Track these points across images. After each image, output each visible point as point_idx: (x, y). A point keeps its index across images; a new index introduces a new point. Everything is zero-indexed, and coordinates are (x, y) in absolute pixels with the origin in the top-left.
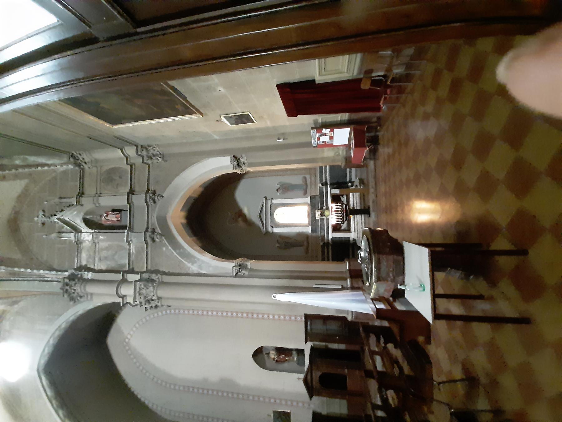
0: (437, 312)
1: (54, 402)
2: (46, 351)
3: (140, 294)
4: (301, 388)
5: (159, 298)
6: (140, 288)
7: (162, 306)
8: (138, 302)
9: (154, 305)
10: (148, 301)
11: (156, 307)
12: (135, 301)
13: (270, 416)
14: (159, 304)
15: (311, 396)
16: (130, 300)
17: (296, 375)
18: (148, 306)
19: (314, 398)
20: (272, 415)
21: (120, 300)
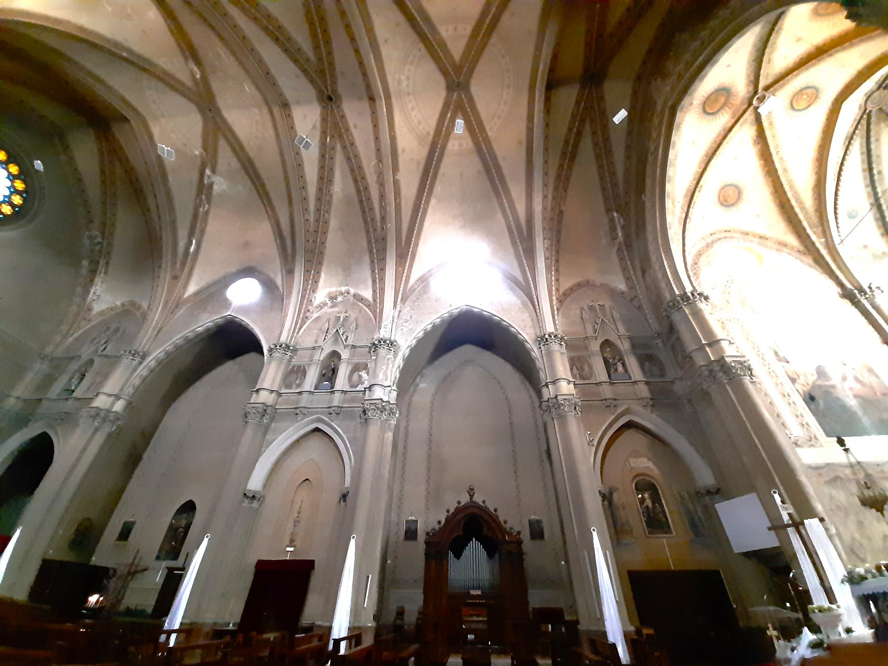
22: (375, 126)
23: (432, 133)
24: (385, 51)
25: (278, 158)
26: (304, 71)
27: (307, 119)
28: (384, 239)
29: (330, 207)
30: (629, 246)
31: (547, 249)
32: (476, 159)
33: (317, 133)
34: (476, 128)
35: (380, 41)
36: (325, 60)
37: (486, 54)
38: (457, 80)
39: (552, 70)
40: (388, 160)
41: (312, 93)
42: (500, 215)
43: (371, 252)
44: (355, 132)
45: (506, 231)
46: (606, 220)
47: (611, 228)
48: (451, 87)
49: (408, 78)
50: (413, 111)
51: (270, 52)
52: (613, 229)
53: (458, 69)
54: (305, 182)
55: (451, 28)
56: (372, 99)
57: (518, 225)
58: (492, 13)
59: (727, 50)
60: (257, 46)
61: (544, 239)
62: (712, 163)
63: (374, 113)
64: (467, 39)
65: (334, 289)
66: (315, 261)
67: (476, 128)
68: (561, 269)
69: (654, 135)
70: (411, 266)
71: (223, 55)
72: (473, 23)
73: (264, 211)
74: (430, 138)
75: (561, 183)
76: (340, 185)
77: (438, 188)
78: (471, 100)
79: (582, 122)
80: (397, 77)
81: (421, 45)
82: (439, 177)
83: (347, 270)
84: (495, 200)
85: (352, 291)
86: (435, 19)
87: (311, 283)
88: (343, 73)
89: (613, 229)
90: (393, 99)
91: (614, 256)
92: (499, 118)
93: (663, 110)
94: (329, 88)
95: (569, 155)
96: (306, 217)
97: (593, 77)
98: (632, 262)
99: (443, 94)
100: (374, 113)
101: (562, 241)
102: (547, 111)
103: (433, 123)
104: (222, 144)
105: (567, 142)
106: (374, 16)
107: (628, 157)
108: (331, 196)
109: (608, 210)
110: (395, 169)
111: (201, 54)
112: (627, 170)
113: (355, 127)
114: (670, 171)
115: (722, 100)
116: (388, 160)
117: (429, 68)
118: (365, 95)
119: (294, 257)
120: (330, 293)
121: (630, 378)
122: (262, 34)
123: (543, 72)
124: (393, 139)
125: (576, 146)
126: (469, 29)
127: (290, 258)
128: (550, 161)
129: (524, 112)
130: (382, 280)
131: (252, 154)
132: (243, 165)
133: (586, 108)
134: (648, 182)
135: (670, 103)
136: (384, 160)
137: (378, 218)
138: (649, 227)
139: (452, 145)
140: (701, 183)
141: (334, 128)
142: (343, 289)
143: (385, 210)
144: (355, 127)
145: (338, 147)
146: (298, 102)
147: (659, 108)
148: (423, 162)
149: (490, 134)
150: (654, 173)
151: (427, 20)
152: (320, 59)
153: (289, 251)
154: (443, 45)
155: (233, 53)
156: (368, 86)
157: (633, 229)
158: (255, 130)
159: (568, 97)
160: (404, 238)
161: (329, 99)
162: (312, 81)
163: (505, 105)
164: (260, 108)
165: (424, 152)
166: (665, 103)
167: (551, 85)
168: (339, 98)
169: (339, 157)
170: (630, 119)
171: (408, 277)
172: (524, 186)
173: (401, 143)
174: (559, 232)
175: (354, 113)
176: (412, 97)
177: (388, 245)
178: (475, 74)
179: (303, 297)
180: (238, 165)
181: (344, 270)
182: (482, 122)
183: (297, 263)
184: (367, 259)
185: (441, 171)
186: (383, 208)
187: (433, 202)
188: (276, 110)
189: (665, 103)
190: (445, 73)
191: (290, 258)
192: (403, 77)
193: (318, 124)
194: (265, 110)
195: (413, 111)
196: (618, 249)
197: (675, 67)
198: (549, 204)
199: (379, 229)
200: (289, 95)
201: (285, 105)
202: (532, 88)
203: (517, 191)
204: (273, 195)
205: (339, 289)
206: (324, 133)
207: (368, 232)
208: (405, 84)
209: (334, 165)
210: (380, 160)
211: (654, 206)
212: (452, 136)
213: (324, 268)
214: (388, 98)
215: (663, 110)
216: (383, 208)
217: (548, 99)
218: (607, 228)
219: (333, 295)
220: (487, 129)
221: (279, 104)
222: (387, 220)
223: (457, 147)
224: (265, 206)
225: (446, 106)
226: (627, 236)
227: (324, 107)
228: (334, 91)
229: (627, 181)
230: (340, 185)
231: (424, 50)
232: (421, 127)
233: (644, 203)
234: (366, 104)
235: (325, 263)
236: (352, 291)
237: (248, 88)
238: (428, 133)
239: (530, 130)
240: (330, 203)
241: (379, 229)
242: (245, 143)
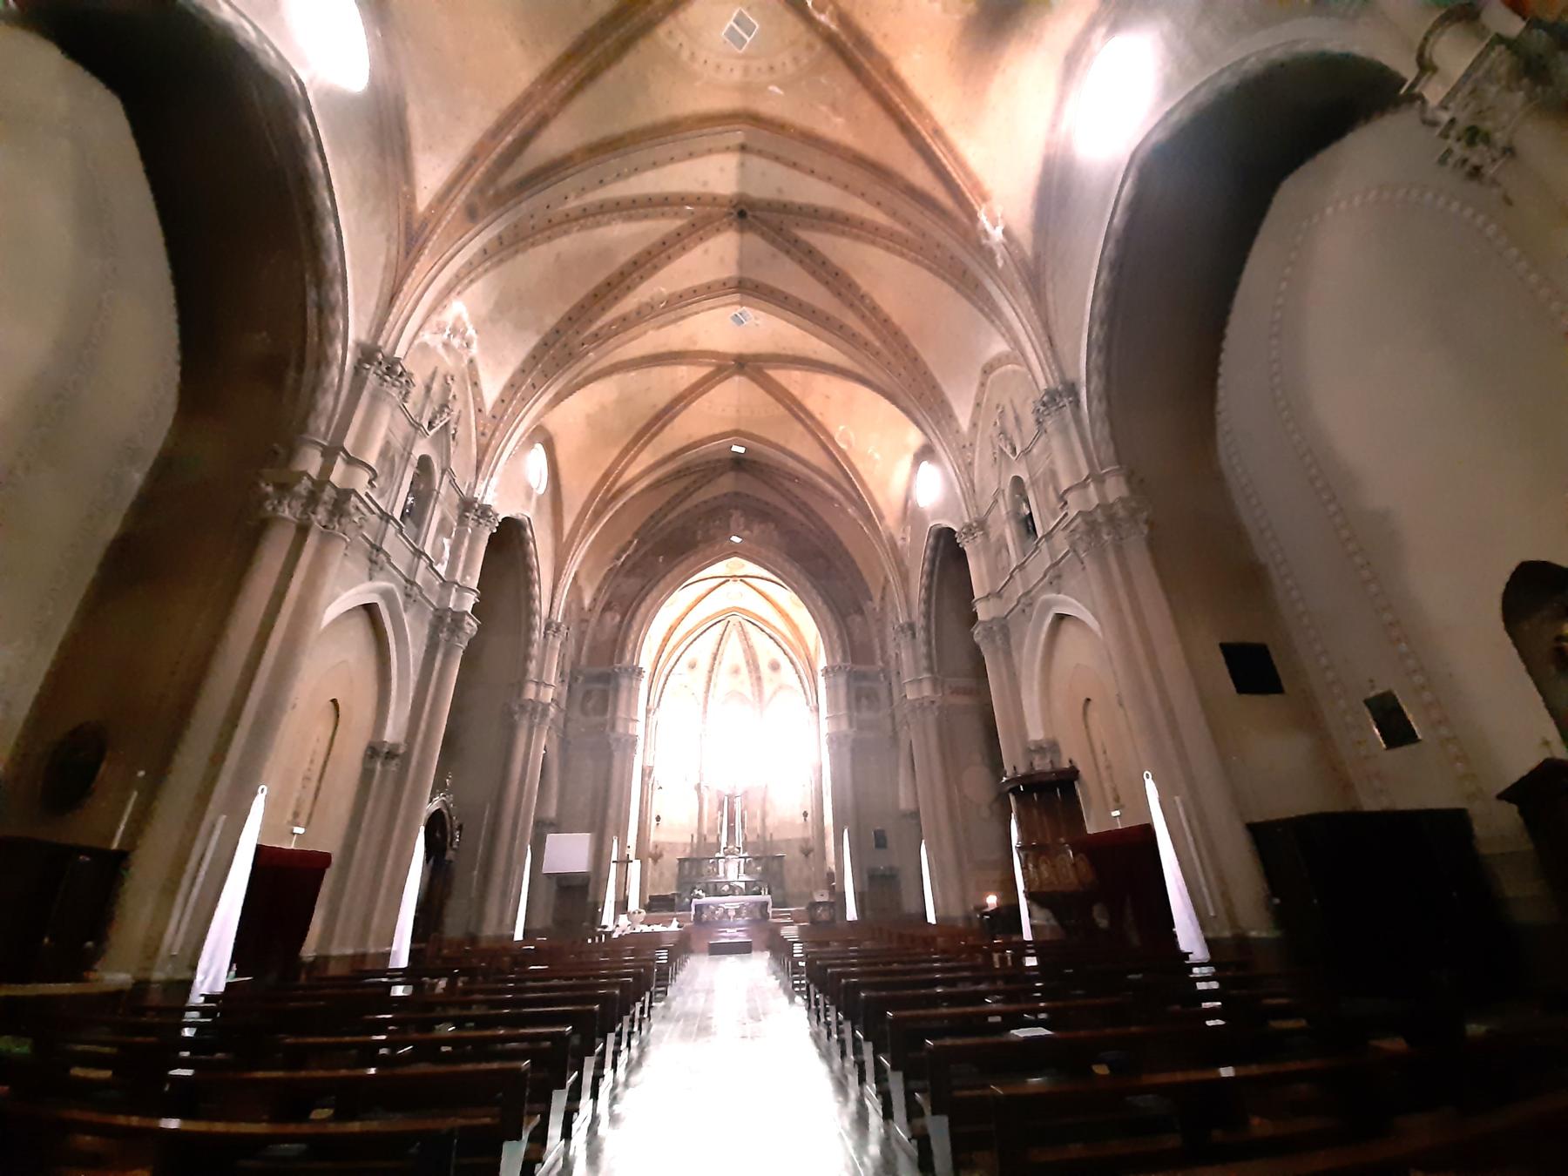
0: (454, 927)
1: (1110, 245)
2: (1175, 117)
3: (1473, 92)
4: (1520, 762)
5: (1509, 151)
6: (1489, 72)
7: (1494, 182)
8: (1445, 117)
9: (1475, 160)
10: (1473, 135)
11: (1476, 173)
12: (1443, 106)
13: (1373, 688)
14: (1490, 171)
15: (1509, 795)
16: (1434, 92)
17: (1552, 733)
18: (1459, 150)
19: (1510, 812)
20: (1379, 691)
21: (1408, 71)
23: (697, 348)
42: (615, 452)
46: (629, 537)
72: (799, 398)
74: (692, 348)
76: (686, 375)
83: (505, 308)
84: (631, 436)
89: (624, 551)
96: (572, 196)
104: (780, 376)
109: (636, 534)
121: (416, 541)
144: (706, 251)
145: (678, 223)
181: (497, 304)
184: (533, 340)
203: (646, 459)
206: (698, 200)
228: (752, 228)
230: (628, 237)
236: (475, 350)
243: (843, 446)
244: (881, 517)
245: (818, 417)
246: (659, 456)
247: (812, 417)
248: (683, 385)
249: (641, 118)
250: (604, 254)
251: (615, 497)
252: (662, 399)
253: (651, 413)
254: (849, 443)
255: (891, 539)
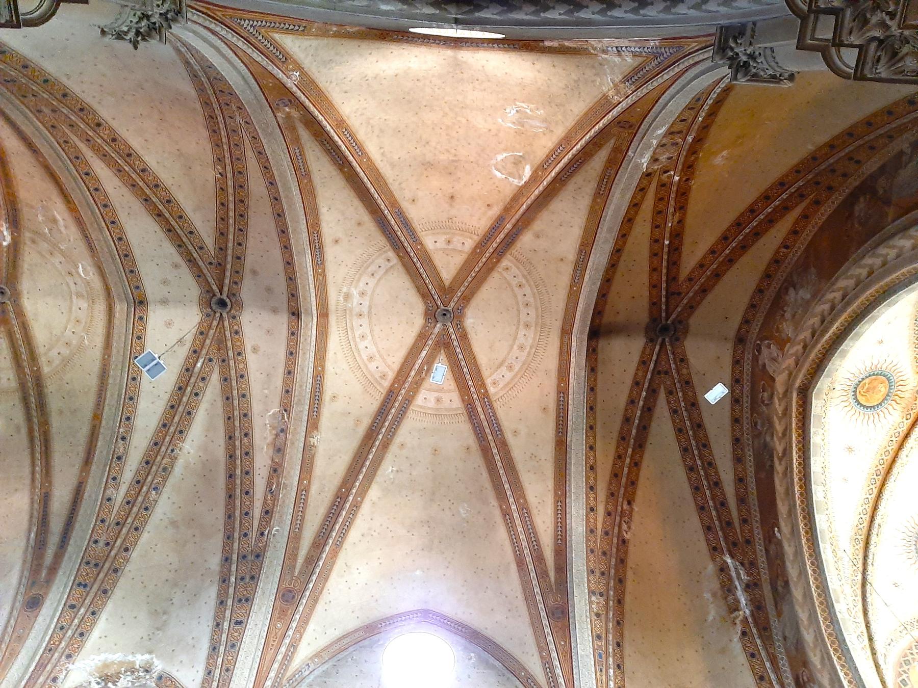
22: (291, 354)
23: (391, 376)
24: (331, 253)
25: (94, 382)
26: (191, 261)
27: (172, 328)
28: (259, 556)
29: (165, 479)
30: (764, 629)
31: (598, 615)
32: (464, 428)
33: (183, 352)
34: (468, 378)
35: (327, 239)
36: (230, 252)
37: (494, 280)
38: (445, 308)
39: (598, 312)
40: (301, 410)
41: (194, 290)
42: (502, 533)
43: (224, 580)
44: (252, 361)
45: (514, 567)
46: (711, 568)
47: (723, 586)
48: (431, 315)
49: (363, 294)
50: (366, 327)
51: (142, 232)
52: (727, 589)
53: (447, 292)
54: (130, 429)
55: (442, 239)
56: (295, 314)
57: (539, 558)
58: (506, 231)
59: (874, 319)
60: (123, 217)
61: (592, 592)
62: (890, 486)
63: (293, 334)
64: (464, 257)
65: (118, 657)
66: (99, 577)
67: (468, 378)
68: (628, 664)
69: (779, 427)
70: (305, 621)
71: (61, 222)
73: (27, 470)
74: (386, 384)
75: (622, 486)
76: (200, 439)
77: (387, 469)
78: (464, 337)
79: (653, 392)
80: (345, 290)
81: (391, 254)
82: (394, 448)
84: (494, 502)
85: (159, 666)
86: (417, 225)
87: (71, 636)
88: (254, 272)
89: (727, 589)
90: (332, 319)
91: (736, 646)
92: (510, 368)
93: (787, 393)
94: (226, 289)
95: (633, 439)
97: (666, 326)
98: (773, 660)
99: (419, 321)
100: (293, 334)
101: (628, 599)
102: (592, 369)
103: (396, 360)
105: (627, 420)
106: (323, 210)
107: (738, 460)
108: (174, 459)
109: (715, 550)
110: (313, 424)
111: (26, 213)
112: (740, 480)
113: (255, 350)
114: (818, 493)
115: (883, 390)
116: (301, 410)
117: (400, 282)
118: (285, 306)
119: (53, 570)
120: (106, 665)
122: (137, 205)
123: (585, 310)
124: (319, 378)
125: (644, 429)
126: (469, 244)
127: (44, 573)
128: (599, 446)
129: (551, 360)
130: (233, 646)
131: (46, 370)
132: (23, 386)
133: (657, 372)
134: (782, 508)
135: (798, 383)
136: (295, 410)
137: (257, 512)
138: (797, 593)
139: (424, 399)
140: (878, 520)
141: (217, 344)
142: (140, 659)
143: (275, 498)
144: (255, 350)
145: (215, 378)
146: (164, 302)
147: (780, 388)
148: (366, 422)
149: (492, 390)
150: (789, 492)
151: (406, 223)
152: (222, 249)
153: (54, 539)
154: (427, 259)
155: (79, 222)
156: (293, 295)
157: (767, 589)
158: (68, 333)
159: (625, 355)
160: (300, 560)
161: (220, 301)
162: (199, 275)
163: (521, 351)
164: (92, 301)
165: (372, 404)
166: (791, 376)
167: (596, 333)
168: (240, 306)
169: (212, 391)
170: (734, 399)
171: (294, 646)
172: (550, 484)
173: (331, 384)
174: (621, 581)
175: (260, 334)
176: (364, 321)
177: (259, 591)
178: (474, 303)
179: (41, 666)
180: (14, 384)
182: (479, 372)
183: (54, 588)
185: (398, 440)
186: (271, 492)
187: (374, 493)
188: (120, 309)
189: (791, 376)
190: (425, 294)
191: (44, 573)
192: (355, 292)
193: (189, 338)
194: (100, 307)
195: (366, 327)
196: (744, 633)
197: (797, 332)
198: (600, 526)
199: (254, 534)
200: (151, 288)
201: (141, 302)
202: (566, 332)
204: (58, 447)
205: (130, 658)
207: (229, 537)
208: (356, 299)
209: (197, 407)
210: (286, 408)
211: (798, 552)
212: (425, 385)
213: (110, 605)
214: (324, 314)
215: (787, 393)
216: (271, 492)
217: (592, 352)
218: (715, 585)
219: (111, 671)
220: (488, 382)
221: (128, 295)
222: (276, 516)
223: (431, 404)
224: (33, 465)
225: (422, 337)
226: (758, 607)
227: (208, 315)
229: (742, 500)
230: (200, 439)
231: (395, 260)
232: (372, 366)
233: (779, 544)
234: (282, 322)
235: (118, 593)
237: (85, 270)
238: (384, 376)
239: (562, 392)
240: (167, 471)
241: (254, 534)
242: (41, 350)
243: (527, 172)
244: (604, 105)
245: (496, 211)
246: (549, 470)
247: (499, 221)
248: (453, 400)
249: (88, 404)
250: (205, 471)
251: (562, 566)
252: (461, 433)
253: (477, 460)
254: (518, 162)
255: (635, 77)
